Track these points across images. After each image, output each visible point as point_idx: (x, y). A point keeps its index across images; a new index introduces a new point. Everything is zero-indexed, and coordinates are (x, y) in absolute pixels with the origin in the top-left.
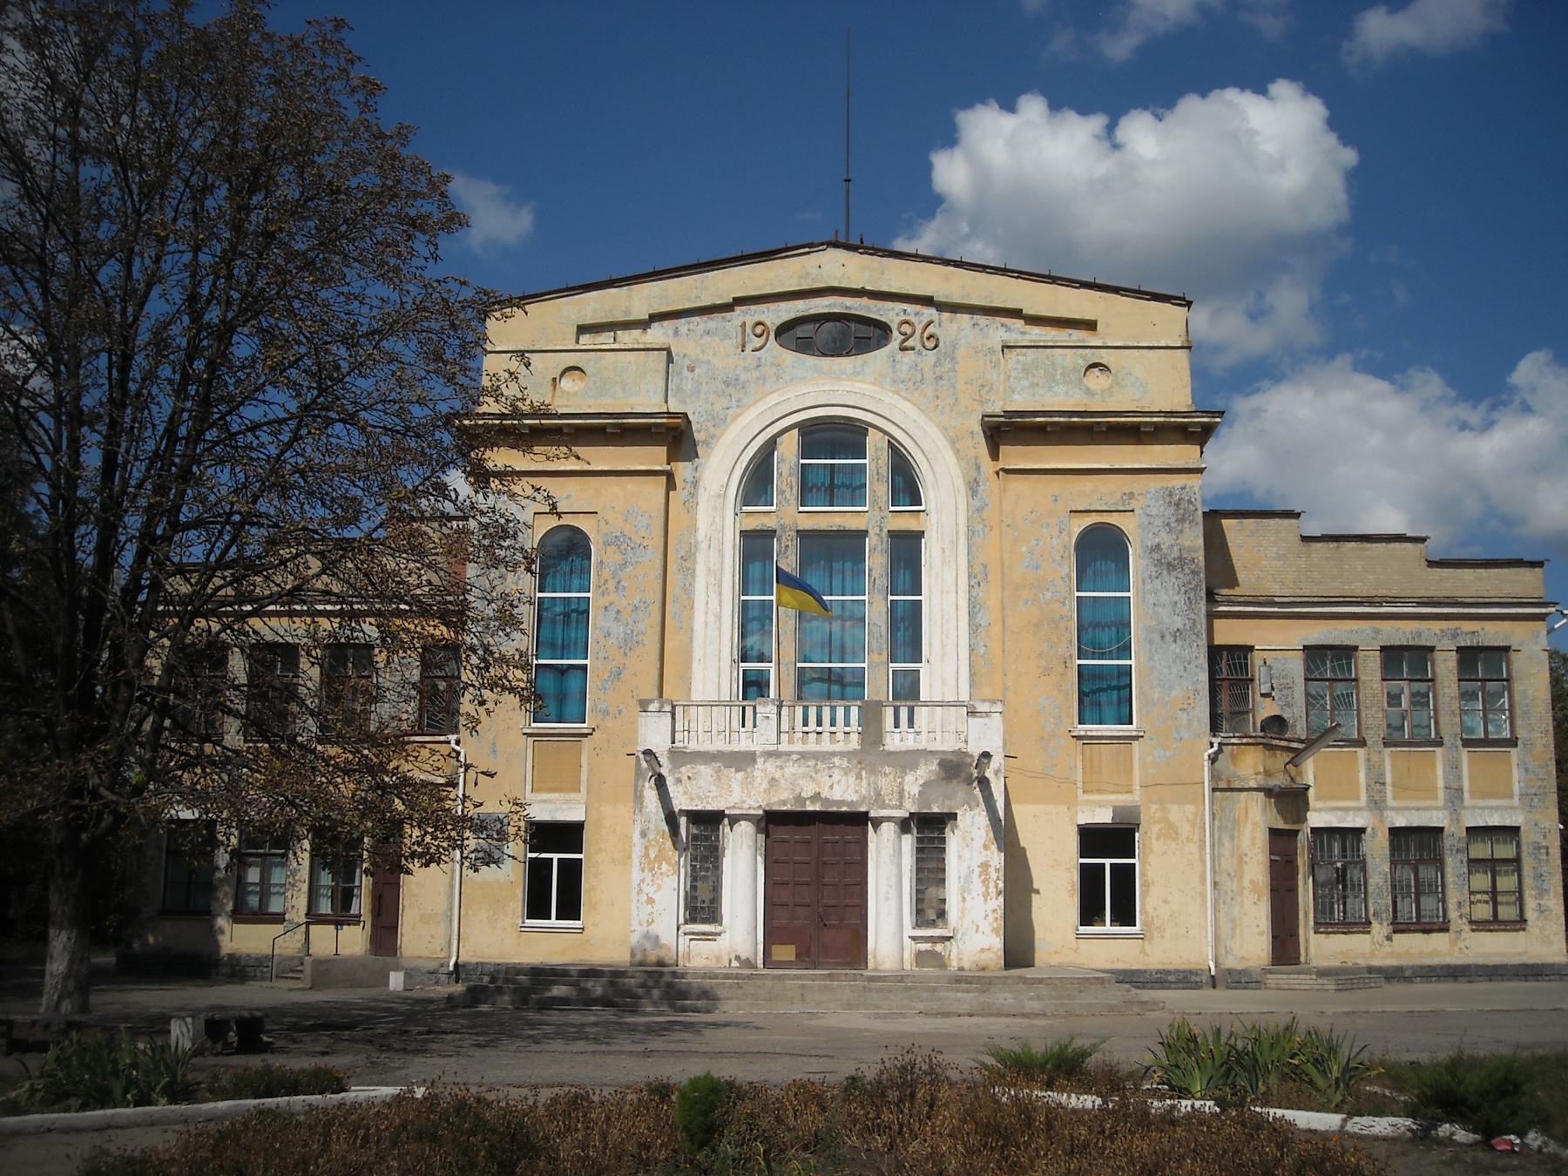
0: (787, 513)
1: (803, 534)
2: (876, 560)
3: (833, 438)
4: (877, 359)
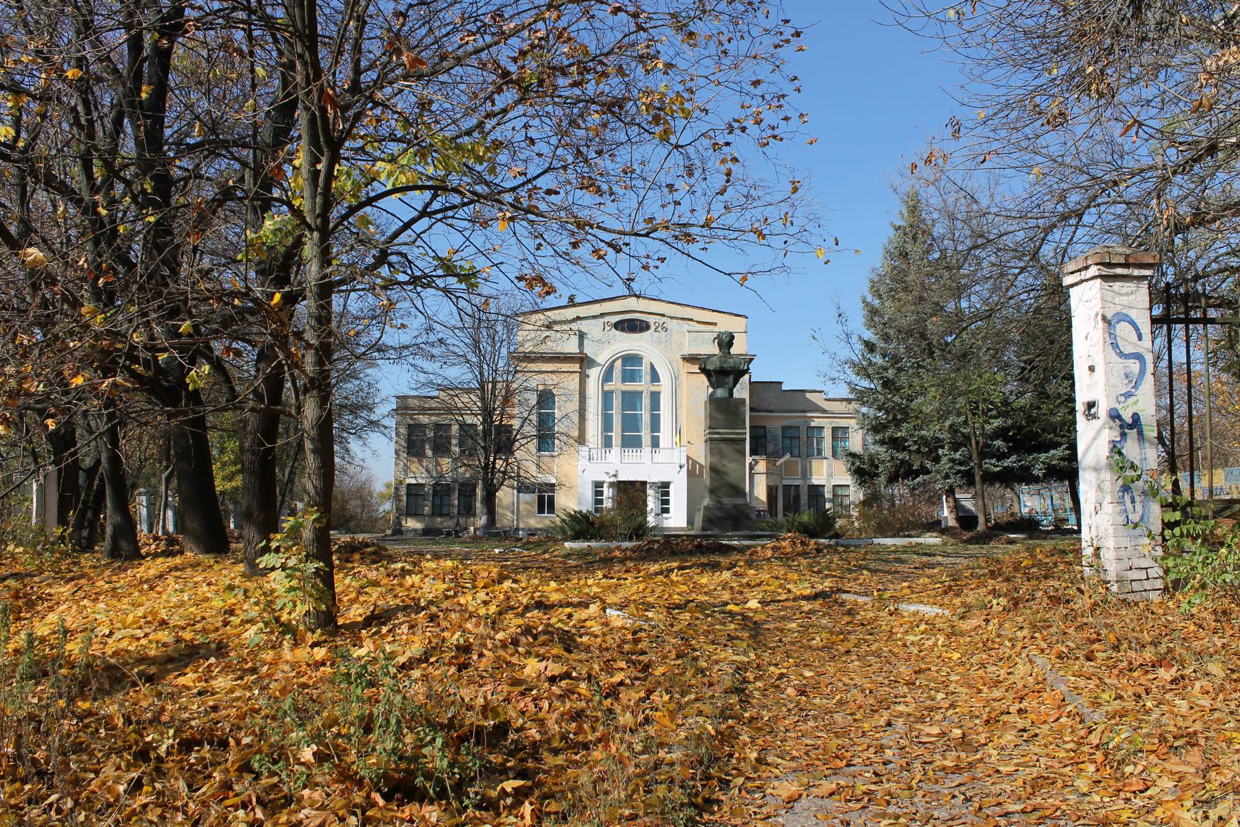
0: (616, 385)
1: (624, 393)
2: (646, 400)
3: (631, 360)
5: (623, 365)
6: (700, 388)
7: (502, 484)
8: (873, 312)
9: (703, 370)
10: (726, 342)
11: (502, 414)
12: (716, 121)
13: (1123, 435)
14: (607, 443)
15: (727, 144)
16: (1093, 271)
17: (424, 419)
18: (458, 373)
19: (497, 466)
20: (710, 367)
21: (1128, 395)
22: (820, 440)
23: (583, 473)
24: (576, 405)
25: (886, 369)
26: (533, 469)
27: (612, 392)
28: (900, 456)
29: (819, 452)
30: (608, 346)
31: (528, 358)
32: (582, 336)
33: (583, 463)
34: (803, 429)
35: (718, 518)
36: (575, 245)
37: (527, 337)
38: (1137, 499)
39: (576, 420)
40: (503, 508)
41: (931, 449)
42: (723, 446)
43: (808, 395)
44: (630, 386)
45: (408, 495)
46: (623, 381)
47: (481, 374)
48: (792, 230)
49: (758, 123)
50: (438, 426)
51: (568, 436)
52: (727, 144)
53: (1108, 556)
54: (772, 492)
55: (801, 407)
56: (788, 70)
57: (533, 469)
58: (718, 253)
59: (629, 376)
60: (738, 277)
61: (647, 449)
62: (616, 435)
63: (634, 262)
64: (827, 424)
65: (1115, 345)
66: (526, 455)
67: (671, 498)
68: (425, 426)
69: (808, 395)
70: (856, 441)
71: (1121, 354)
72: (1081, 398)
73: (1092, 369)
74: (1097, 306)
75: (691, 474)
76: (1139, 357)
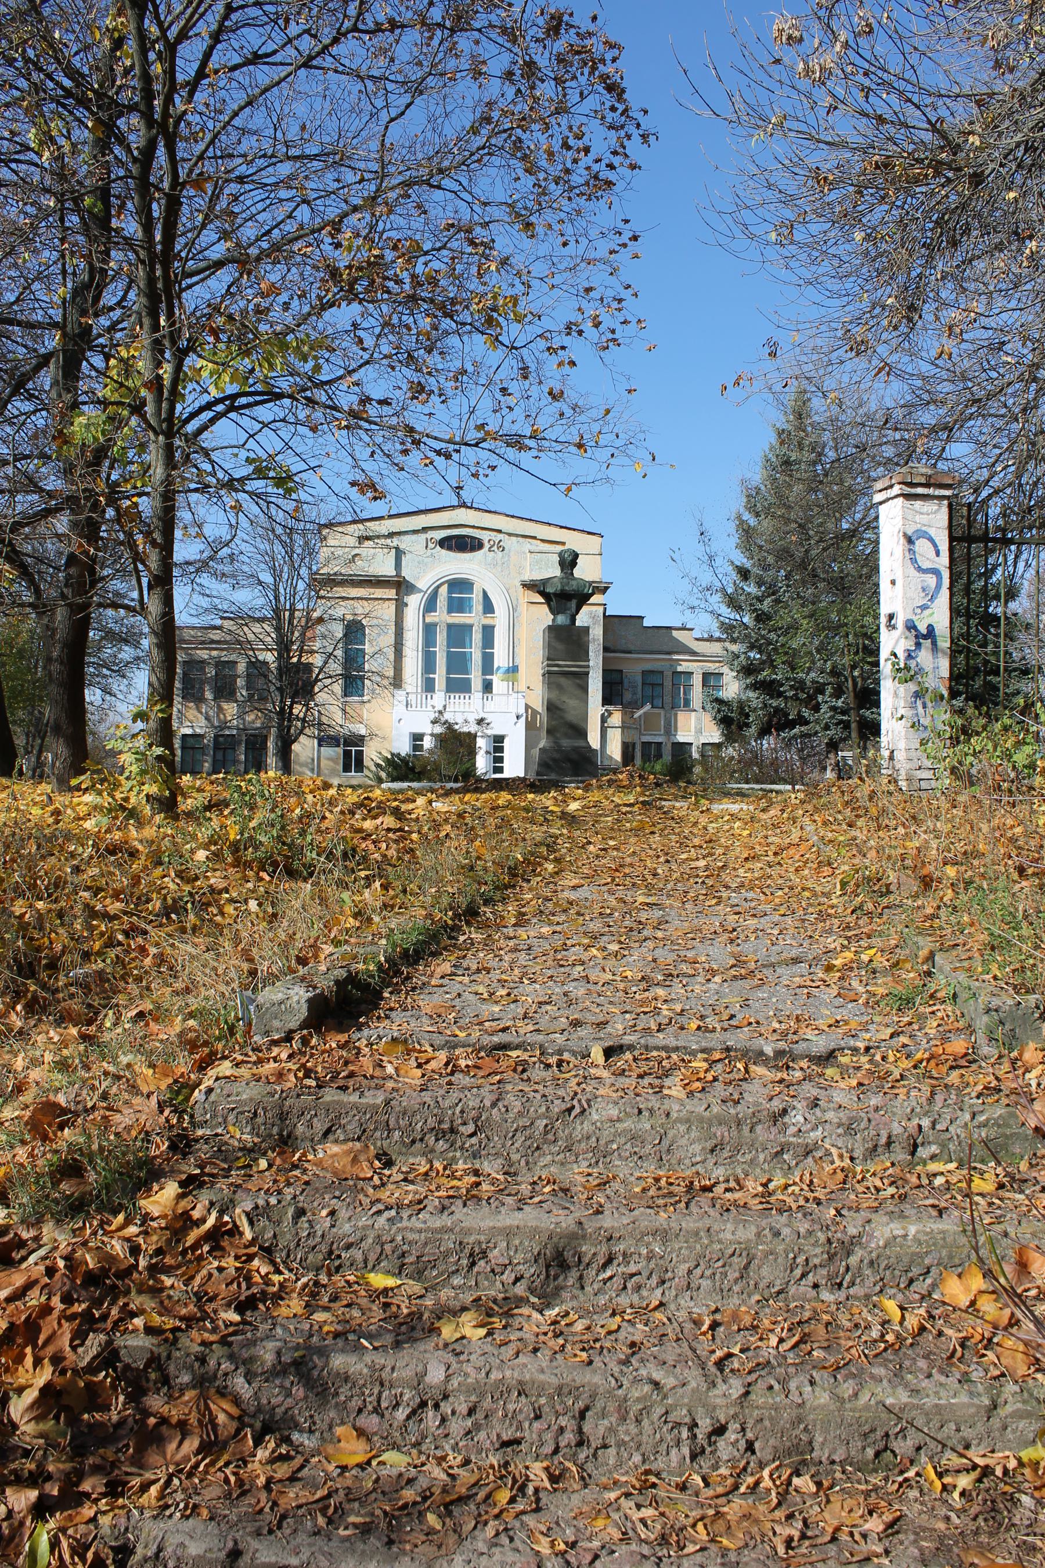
0: (441, 616)
1: (450, 627)
2: (477, 636)
3: (460, 585)
4: (479, 554)
5: (450, 592)
6: (540, 617)
7: (301, 732)
8: (747, 534)
9: (543, 594)
10: (569, 561)
11: (301, 651)
12: (555, 322)
13: (918, 645)
14: (429, 687)
15: (563, 348)
16: (896, 490)
17: (204, 654)
18: (249, 598)
19: (295, 711)
20: (550, 590)
21: (924, 608)
22: (688, 687)
23: (398, 720)
24: (391, 639)
25: (760, 600)
26: (338, 717)
27: (435, 625)
28: (774, 703)
29: (687, 703)
30: (430, 569)
31: (332, 581)
32: (399, 553)
33: (400, 709)
34: (668, 674)
35: (554, 760)
36: (405, 452)
37: (337, 551)
38: (929, 705)
39: (392, 657)
40: (301, 765)
41: (811, 697)
42: (563, 680)
43: (675, 633)
44: (458, 618)
45: (183, 748)
46: (450, 611)
47: (277, 598)
48: (618, 443)
49: (597, 325)
50: (220, 664)
51: (383, 676)
52: (563, 348)
53: (900, 756)
54: (628, 750)
55: (665, 648)
56: (625, 276)
57: (338, 717)
58: (547, 466)
59: (457, 606)
60: (563, 488)
61: (477, 695)
62: (440, 676)
63: (463, 470)
64: (697, 669)
65: (914, 561)
66: (329, 699)
67: (506, 755)
68: (203, 662)
69: (675, 633)
70: (732, 688)
71: (919, 569)
72: (884, 610)
73: (893, 582)
74: (899, 522)
75: (530, 726)
76: (936, 572)
